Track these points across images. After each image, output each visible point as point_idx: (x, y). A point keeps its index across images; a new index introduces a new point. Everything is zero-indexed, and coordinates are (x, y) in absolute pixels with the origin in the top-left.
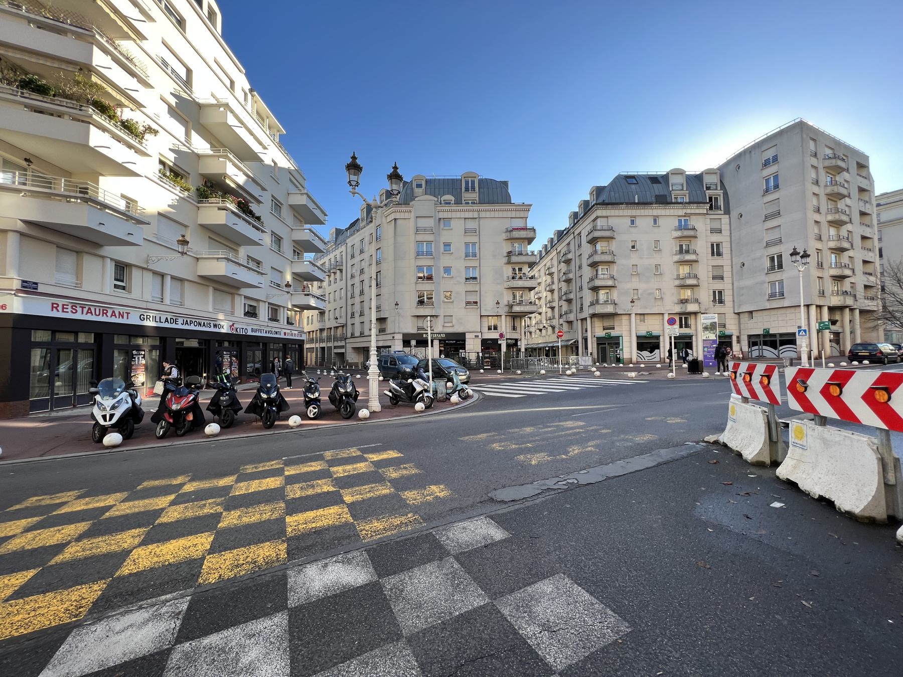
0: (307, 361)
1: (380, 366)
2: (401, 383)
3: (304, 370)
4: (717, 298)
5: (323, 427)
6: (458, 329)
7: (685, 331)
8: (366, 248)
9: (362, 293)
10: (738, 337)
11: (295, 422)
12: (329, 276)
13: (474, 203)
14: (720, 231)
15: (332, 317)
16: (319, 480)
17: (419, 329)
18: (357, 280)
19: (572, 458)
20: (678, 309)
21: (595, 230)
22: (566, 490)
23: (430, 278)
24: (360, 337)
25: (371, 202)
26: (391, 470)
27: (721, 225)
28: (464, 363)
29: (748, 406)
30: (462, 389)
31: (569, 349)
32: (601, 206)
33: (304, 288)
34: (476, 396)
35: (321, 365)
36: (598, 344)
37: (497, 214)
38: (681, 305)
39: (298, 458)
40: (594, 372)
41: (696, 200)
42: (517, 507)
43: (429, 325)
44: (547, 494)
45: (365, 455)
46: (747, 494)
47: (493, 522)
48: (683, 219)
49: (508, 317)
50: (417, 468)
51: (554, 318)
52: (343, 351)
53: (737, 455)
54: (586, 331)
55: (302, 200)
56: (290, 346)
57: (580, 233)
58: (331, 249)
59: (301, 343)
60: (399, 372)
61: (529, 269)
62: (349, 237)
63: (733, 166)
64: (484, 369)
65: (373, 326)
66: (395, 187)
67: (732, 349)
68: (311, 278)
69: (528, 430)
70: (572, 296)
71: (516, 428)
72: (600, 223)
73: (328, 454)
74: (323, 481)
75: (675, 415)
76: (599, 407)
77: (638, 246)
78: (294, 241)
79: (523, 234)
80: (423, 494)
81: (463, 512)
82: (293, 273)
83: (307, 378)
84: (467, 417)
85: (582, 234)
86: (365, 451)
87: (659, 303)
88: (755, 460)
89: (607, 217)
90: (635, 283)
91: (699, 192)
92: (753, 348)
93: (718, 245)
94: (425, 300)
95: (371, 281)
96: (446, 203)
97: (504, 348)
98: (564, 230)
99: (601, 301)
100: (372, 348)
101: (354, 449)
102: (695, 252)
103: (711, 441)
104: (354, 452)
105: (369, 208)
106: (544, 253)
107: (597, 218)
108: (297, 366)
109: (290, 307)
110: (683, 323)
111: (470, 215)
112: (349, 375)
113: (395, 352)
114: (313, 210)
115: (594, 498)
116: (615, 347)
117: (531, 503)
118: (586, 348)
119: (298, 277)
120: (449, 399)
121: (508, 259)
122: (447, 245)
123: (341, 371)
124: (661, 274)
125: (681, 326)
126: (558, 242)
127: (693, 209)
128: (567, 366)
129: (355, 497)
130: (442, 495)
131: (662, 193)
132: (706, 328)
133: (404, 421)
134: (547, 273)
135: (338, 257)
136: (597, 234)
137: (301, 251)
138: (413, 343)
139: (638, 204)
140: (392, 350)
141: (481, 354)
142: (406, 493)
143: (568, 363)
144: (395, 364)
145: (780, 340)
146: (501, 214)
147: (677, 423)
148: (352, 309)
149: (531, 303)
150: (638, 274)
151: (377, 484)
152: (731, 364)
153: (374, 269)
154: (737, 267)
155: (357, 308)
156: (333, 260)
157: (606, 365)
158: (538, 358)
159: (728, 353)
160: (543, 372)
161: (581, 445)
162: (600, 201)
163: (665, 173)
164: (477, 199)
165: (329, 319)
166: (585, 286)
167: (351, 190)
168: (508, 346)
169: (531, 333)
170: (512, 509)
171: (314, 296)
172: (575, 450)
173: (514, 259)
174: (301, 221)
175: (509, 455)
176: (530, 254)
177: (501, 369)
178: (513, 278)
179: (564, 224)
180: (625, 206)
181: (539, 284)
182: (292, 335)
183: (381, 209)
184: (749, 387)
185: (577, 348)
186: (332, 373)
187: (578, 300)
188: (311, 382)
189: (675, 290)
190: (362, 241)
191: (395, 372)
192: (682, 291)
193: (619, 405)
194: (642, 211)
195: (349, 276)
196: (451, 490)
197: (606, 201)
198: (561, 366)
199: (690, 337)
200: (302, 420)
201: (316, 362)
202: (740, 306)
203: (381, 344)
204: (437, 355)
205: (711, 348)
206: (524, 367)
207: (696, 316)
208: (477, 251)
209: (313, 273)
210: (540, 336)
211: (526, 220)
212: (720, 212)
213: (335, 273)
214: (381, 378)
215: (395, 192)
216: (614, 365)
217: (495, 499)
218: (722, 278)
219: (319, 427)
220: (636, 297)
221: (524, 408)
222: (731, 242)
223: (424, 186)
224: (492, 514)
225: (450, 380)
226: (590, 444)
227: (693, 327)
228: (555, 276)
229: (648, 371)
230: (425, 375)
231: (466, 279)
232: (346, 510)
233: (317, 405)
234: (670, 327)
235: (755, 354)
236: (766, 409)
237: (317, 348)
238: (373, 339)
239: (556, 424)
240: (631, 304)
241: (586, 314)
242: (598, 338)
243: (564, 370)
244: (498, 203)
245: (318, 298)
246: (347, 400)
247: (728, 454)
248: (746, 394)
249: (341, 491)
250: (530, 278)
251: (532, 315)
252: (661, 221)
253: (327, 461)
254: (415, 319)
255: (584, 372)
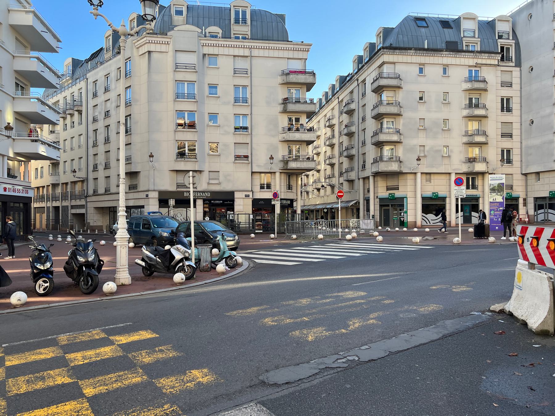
0: (35, 224)
1: (130, 230)
2: (156, 250)
3: (31, 234)
4: (505, 158)
5: (57, 304)
6: (226, 187)
7: (472, 192)
8: (112, 86)
9: (107, 141)
10: (525, 200)
11: (19, 300)
12: (64, 118)
13: (244, 38)
14: (510, 85)
15: (68, 168)
16: (51, 370)
17: (178, 186)
18: (101, 125)
19: (354, 332)
20: (465, 168)
21: (381, 78)
22: (346, 369)
23: (192, 126)
24: (105, 195)
25: (120, 29)
26: (143, 354)
27: (512, 78)
28: (232, 226)
29: (535, 272)
30: (229, 256)
31: (350, 211)
32: (388, 50)
33: (31, 132)
34: (246, 264)
35: (55, 228)
36: (381, 206)
37: (272, 53)
38: (469, 164)
39: (23, 344)
40: (376, 236)
41: (487, 50)
42: (291, 390)
43: (191, 182)
44: (326, 374)
45: (111, 338)
46: (532, 364)
47: (265, 409)
48: (473, 69)
49: (283, 175)
50: (176, 350)
51: (333, 176)
52: (82, 211)
53: (522, 324)
54: (369, 191)
55: (27, 20)
56: (12, 204)
57: (364, 81)
58: (66, 84)
59: (27, 202)
60: (154, 237)
61: (307, 120)
62: (90, 71)
63: (525, 14)
64: (255, 234)
65: (122, 181)
66: (149, 11)
67: (518, 213)
68: (42, 120)
69: (305, 301)
70: (354, 152)
71: (291, 300)
72: (386, 69)
73: (63, 338)
74: (57, 371)
75: (461, 283)
76: (381, 275)
77: (425, 98)
78: (16, 72)
79: (301, 78)
80: (183, 380)
81: (230, 399)
82: (16, 113)
83: (34, 244)
84: (235, 288)
85: (367, 82)
86: (111, 332)
87: (446, 161)
88: (540, 329)
89: (394, 63)
90: (421, 139)
91: (490, 41)
92: (540, 212)
93: (508, 100)
94: (187, 151)
95: (118, 127)
96: (212, 36)
97: (278, 210)
98: (348, 76)
99: (385, 159)
100: (120, 208)
101: (97, 330)
102: (484, 107)
103: (497, 310)
104: (97, 334)
105: (116, 36)
106: (324, 102)
107: (383, 63)
108: (22, 230)
109: (11, 155)
110: (471, 184)
111: (241, 52)
112: (90, 240)
113: (149, 213)
114: (42, 34)
115: (376, 376)
116: (399, 209)
117: (308, 385)
118: (368, 210)
119: (21, 117)
120: (215, 269)
121: (284, 107)
122: (213, 87)
123: (81, 237)
124: (449, 130)
125: (468, 188)
126: (340, 89)
127: (484, 59)
128: (347, 230)
129: (97, 389)
130: (205, 380)
131: (453, 39)
132: (493, 190)
133: (160, 295)
134: (327, 124)
135: (76, 94)
136: (383, 82)
137: (26, 85)
138: (172, 202)
139: (428, 50)
140: (146, 210)
141: (251, 217)
142: (161, 381)
143: (348, 227)
144: (149, 228)
145: (549, 204)
146: (276, 54)
147: (463, 292)
148: (95, 160)
149: (308, 158)
150: (425, 129)
151: (126, 372)
152: (518, 228)
153: (122, 112)
154: (526, 124)
155: (101, 159)
156: (69, 98)
157: (389, 229)
158: (315, 221)
159: (514, 217)
160: (321, 236)
161: (362, 318)
162: (387, 44)
163: (457, 17)
164: (249, 33)
165: (64, 172)
166: (369, 141)
167: (93, 11)
168: (283, 207)
169: (308, 193)
170: (286, 392)
171: (43, 143)
172: (355, 324)
173: (291, 107)
174: (25, 47)
175: (284, 330)
176: (309, 102)
177: (274, 234)
178: (289, 129)
179: (348, 69)
180: (414, 51)
181: (318, 137)
182: (14, 191)
183: (130, 39)
184: (536, 253)
185: (358, 210)
186: (69, 239)
187: (361, 157)
188: (40, 250)
189: (462, 148)
190: (107, 76)
191: (149, 238)
192: (470, 149)
193: (402, 273)
194: (427, 58)
195: (90, 119)
196: (216, 374)
197: (394, 45)
198: (340, 230)
199: (477, 199)
200: (28, 297)
201: (47, 225)
202: (527, 166)
203: (131, 203)
204: (200, 217)
205: (497, 211)
206: (300, 230)
207: (450, 175)
208: (248, 96)
209: (43, 113)
210: (318, 196)
211: (305, 62)
212: (511, 64)
213: (72, 115)
214: (132, 245)
215: (150, 18)
216: (397, 229)
217: (266, 381)
218: (511, 136)
219: (51, 305)
220: (422, 155)
221: (298, 278)
222: (521, 97)
223: (185, 13)
224: (262, 399)
225: (216, 246)
226: (371, 316)
227: (480, 188)
228: (336, 129)
229: (433, 236)
230: (186, 240)
231: (236, 129)
232: (86, 405)
233: (49, 278)
234: (457, 187)
235: (541, 217)
236: (551, 275)
237: (48, 208)
238: (122, 197)
239: (335, 294)
240: (416, 162)
241: (368, 172)
242: (381, 200)
243: (344, 234)
244: (273, 40)
245: (49, 145)
246: (88, 271)
247: (513, 323)
248: (533, 260)
249: (80, 383)
250: (308, 130)
251: (310, 173)
252: (451, 71)
253: (62, 347)
254: (174, 174)
255: (365, 236)
